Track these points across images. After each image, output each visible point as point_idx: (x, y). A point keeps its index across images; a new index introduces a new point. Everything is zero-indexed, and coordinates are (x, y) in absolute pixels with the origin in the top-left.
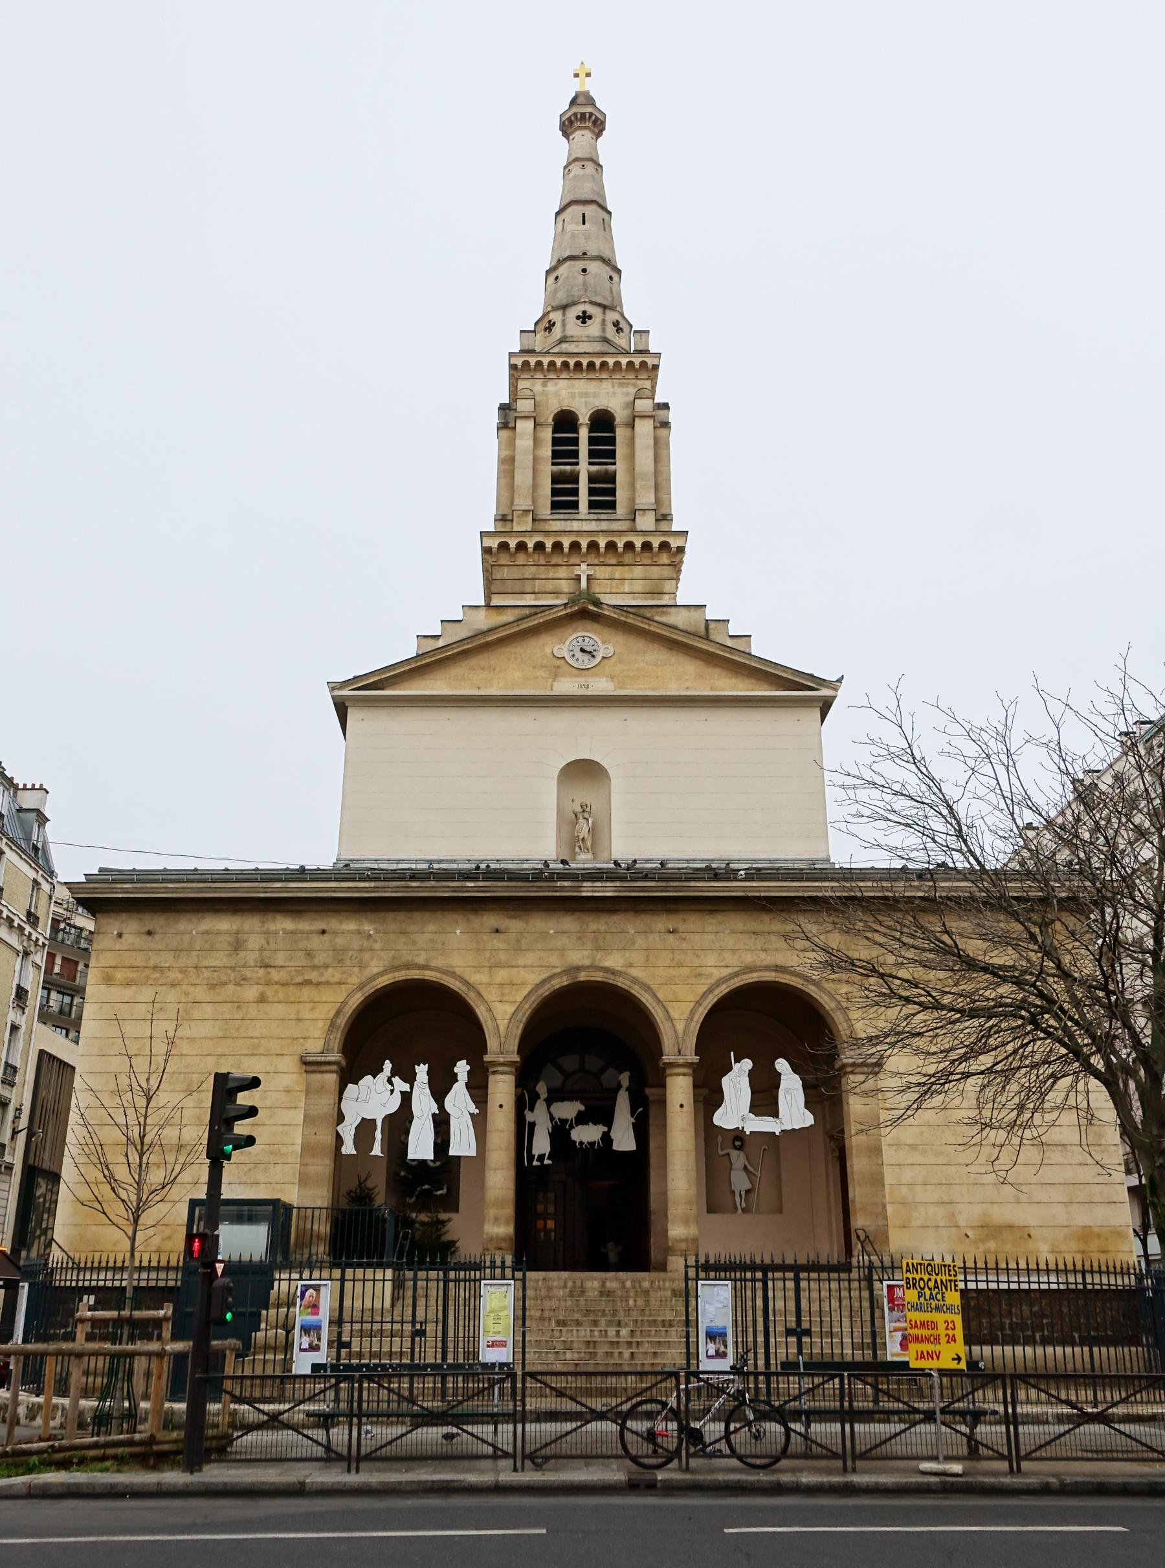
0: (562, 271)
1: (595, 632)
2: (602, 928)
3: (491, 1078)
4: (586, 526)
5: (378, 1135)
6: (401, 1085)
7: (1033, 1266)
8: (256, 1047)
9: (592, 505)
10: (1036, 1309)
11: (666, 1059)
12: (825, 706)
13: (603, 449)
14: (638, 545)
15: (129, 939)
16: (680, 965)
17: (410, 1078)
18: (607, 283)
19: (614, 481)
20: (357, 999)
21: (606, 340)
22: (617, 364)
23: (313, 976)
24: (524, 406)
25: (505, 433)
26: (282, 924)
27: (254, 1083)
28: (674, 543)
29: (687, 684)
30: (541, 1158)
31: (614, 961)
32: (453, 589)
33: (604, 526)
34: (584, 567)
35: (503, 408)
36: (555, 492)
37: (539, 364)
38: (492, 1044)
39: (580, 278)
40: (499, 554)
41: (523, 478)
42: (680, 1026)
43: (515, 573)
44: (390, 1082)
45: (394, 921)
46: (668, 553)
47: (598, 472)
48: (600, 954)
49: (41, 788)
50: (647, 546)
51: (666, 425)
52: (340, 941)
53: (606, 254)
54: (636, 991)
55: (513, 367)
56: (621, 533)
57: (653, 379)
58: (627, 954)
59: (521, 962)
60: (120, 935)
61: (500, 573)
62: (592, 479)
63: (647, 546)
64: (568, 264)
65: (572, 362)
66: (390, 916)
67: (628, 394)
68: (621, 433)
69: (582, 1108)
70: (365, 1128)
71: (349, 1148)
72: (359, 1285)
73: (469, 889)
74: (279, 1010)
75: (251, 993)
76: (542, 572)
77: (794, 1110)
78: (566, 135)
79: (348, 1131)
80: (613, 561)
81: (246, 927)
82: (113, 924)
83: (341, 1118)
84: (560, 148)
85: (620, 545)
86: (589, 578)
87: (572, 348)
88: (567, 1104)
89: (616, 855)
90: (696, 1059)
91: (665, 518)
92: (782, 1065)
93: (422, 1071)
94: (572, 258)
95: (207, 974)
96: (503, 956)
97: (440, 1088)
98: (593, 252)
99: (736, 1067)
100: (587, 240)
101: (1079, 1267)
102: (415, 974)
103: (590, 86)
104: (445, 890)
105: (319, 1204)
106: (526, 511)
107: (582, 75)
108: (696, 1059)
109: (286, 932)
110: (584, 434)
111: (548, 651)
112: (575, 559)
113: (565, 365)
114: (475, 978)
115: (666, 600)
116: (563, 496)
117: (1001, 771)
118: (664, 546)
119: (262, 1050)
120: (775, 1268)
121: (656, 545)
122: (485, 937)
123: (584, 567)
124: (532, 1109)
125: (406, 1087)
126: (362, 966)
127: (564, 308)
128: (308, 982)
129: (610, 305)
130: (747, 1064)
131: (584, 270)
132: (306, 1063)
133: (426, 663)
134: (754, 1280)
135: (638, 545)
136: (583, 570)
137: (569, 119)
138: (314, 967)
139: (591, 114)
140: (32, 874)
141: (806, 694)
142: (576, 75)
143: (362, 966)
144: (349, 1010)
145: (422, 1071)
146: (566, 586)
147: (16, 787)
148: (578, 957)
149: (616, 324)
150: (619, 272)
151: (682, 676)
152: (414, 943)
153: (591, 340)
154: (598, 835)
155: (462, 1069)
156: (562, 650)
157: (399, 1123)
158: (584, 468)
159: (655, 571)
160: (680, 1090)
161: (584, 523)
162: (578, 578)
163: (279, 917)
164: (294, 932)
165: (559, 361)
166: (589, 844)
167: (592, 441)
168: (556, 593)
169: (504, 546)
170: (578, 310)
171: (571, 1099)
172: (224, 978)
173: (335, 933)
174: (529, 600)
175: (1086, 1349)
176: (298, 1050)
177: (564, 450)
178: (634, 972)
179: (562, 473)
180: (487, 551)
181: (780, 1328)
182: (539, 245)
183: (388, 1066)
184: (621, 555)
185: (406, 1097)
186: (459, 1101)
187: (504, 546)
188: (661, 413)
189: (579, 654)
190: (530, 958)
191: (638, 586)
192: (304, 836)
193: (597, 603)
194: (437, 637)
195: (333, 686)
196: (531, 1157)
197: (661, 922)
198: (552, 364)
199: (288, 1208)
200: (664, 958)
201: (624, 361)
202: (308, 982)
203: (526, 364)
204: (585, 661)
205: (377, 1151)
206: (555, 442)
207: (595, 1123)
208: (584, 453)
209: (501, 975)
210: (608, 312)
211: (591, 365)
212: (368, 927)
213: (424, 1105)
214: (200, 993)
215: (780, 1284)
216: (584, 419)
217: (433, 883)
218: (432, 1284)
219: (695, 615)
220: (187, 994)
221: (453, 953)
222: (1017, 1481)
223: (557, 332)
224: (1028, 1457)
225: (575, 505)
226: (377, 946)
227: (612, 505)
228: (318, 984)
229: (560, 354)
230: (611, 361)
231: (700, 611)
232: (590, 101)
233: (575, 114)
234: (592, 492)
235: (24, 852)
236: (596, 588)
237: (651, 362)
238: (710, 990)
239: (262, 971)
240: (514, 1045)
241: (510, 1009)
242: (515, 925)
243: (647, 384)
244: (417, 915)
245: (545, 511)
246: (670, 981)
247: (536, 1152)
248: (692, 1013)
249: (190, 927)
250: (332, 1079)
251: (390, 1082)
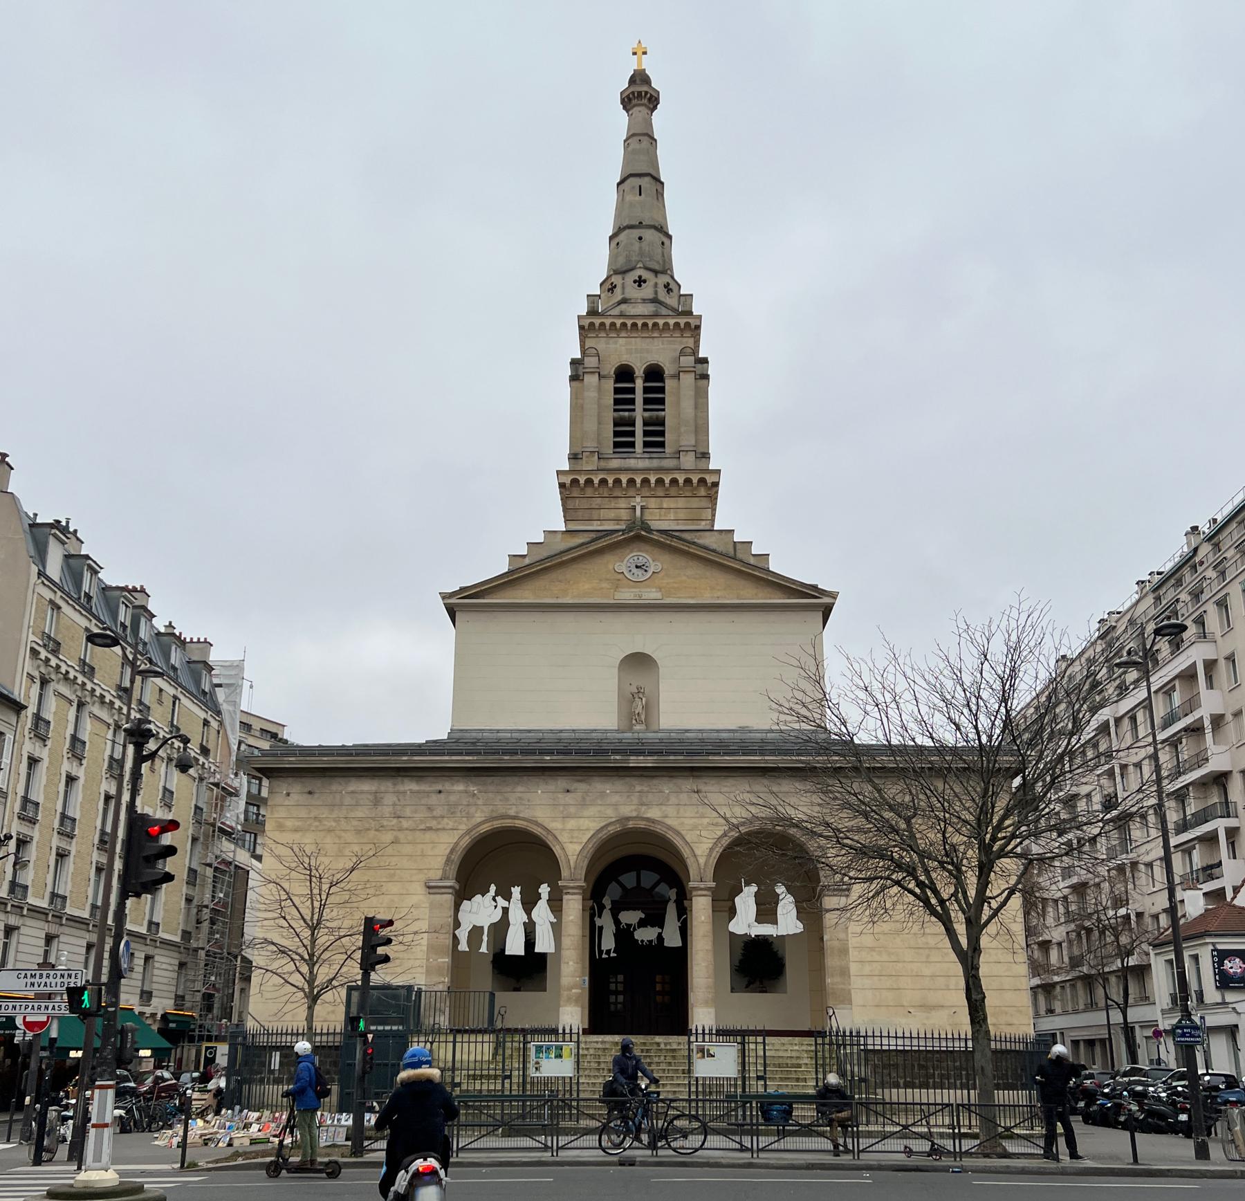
0: (622, 237)
1: (646, 552)
2: (646, 789)
4: (641, 464)
5: (485, 938)
6: (501, 902)
7: (956, 1036)
8: (394, 875)
9: (646, 444)
10: (958, 1064)
11: (691, 884)
12: (827, 611)
13: (655, 398)
14: (681, 481)
15: (295, 797)
16: (702, 817)
17: (508, 897)
19: (663, 424)
20: (466, 841)
21: (655, 301)
22: (666, 324)
23: (433, 824)
24: (591, 362)
25: (575, 384)
26: (410, 786)
27: (391, 923)
28: (710, 479)
29: (719, 594)
30: (608, 952)
31: (654, 813)
33: (655, 463)
34: (638, 499)
35: (574, 363)
36: (616, 434)
37: (602, 324)
38: (565, 873)
39: (637, 244)
40: (570, 488)
42: (702, 861)
43: (584, 504)
44: (494, 899)
45: (492, 783)
46: (707, 487)
47: (651, 417)
48: (644, 808)
49: (205, 641)
50: (688, 481)
51: (706, 377)
55: (581, 328)
56: (667, 470)
58: (664, 808)
60: (288, 794)
61: (570, 505)
63: (688, 481)
64: (627, 231)
65: (629, 322)
66: (490, 780)
67: (675, 350)
68: (669, 384)
69: (643, 916)
70: (476, 932)
71: (463, 946)
72: (465, 1045)
73: (547, 762)
74: (408, 849)
75: (388, 837)
76: (606, 503)
77: (788, 922)
79: (463, 934)
80: (662, 494)
81: (383, 789)
82: (283, 786)
83: (457, 924)
84: (621, 121)
85: (667, 481)
86: (642, 508)
88: (631, 913)
90: (713, 884)
91: (705, 456)
92: (780, 889)
93: (516, 891)
95: (355, 823)
97: (529, 903)
99: (746, 889)
102: (508, 823)
105: (440, 987)
107: (640, 53)
108: (713, 884)
109: (412, 792)
110: (639, 384)
112: (631, 492)
116: (623, 442)
118: (702, 481)
119: (396, 878)
121: (695, 481)
122: (560, 796)
123: (638, 499)
124: (600, 916)
125: (505, 904)
126: (469, 816)
128: (430, 829)
129: (664, 268)
130: (754, 888)
131: (640, 238)
132: (429, 887)
135: (681, 481)
136: (638, 501)
137: (628, 96)
138: (434, 817)
139: (646, 93)
140: (203, 715)
141: (814, 603)
142: (635, 54)
143: (469, 816)
145: (516, 891)
146: (624, 515)
147: (184, 642)
148: (628, 810)
149: (667, 286)
150: (670, 237)
151: (714, 588)
152: (507, 800)
154: (650, 708)
155: (544, 890)
157: (500, 928)
159: (695, 503)
160: (701, 907)
161: (639, 460)
162: (634, 508)
163: (406, 780)
164: (418, 792)
165: (618, 322)
166: (643, 717)
167: (646, 390)
168: (618, 520)
171: (634, 909)
172: (367, 826)
173: (449, 792)
174: (596, 526)
175: (965, 1092)
176: (422, 877)
177: (623, 399)
178: (669, 822)
179: (622, 418)
180: (562, 486)
181: (753, 1075)
183: (493, 888)
184: (667, 490)
185: (505, 911)
186: (542, 913)
187: (575, 482)
189: (635, 570)
190: (592, 811)
192: (426, 721)
193: (649, 530)
194: (523, 556)
195: (445, 596)
196: (601, 952)
200: (690, 812)
202: (430, 829)
203: (592, 324)
204: (640, 575)
205: (484, 949)
207: (652, 926)
208: (639, 393)
209: (572, 824)
210: (651, 296)
212: (473, 788)
213: (517, 916)
214: (349, 837)
215: (752, 1046)
216: (639, 372)
217: (520, 757)
218: (486, 1045)
220: (340, 837)
223: (618, 295)
225: (632, 445)
226: (480, 802)
228: (438, 830)
229: (622, 315)
230: (661, 322)
231: (729, 535)
233: (633, 93)
234: (646, 434)
235: (195, 697)
236: (647, 516)
237: (693, 323)
239: (395, 821)
241: (578, 848)
245: (609, 449)
247: (604, 948)
248: (711, 849)
249: (340, 788)
250: (448, 899)
251: (494, 899)
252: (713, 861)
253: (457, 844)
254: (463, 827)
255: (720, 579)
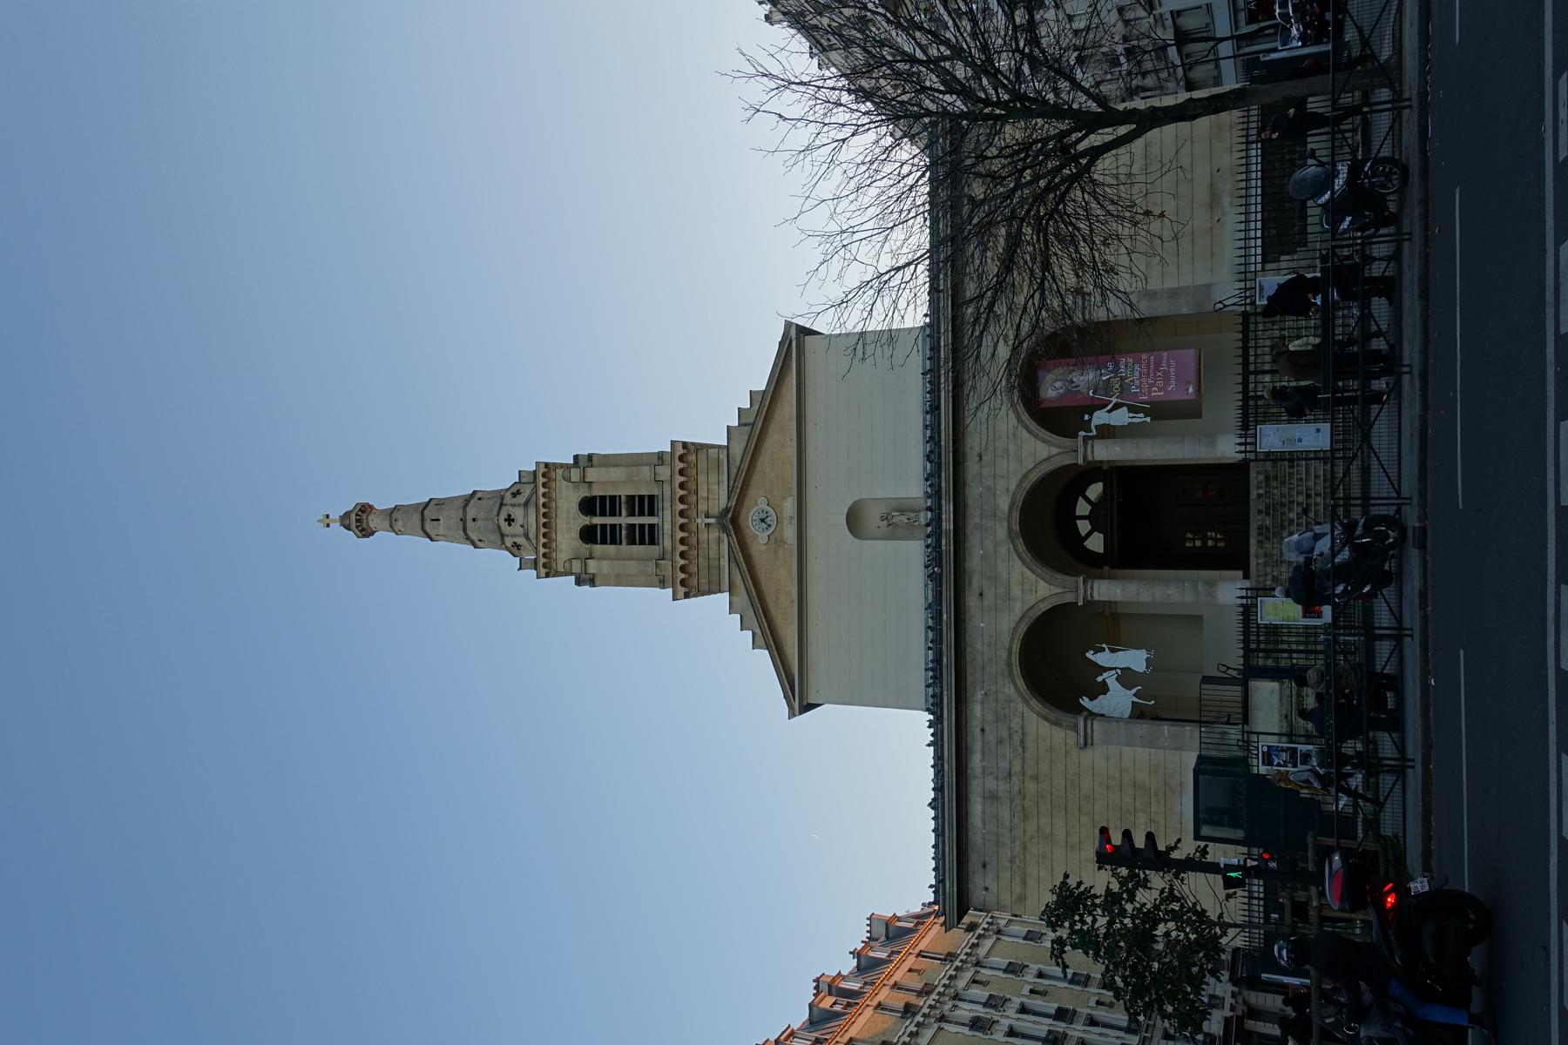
0: (473, 536)
3: (1096, 597)
4: (668, 518)
9: (651, 513)
10: (1277, 165)
12: (804, 332)
13: (608, 505)
15: (989, 882)
16: (1007, 451)
18: (484, 502)
21: (526, 504)
22: (544, 495)
23: (1017, 738)
25: (597, 581)
26: (976, 762)
27: (1104, 831)
28: (680, 451)
31: (1004, 503)
32: (715, 613)
33: (667, 504)
35: (579, 582)
36: (642, 542)
37: (544, 555)
39: (479, 523)
40: (689, 586)
41: (616, 474)
42: (1054, 451)
46: (687, 454)
50: (682, 472)
51: (590, 457)
52: (989, 717)
53: (460, 503)
54: (1027, 485)
57: (556, 466)
59: (1005, 576)
61: (705, 587)
62: (631, 514)
68: (597, 492)
75: (1031, 786)
78: (372, 533)
81: (979, 790)
84: (383, 537)
85: (682, 493)
86: (707, 516)
87: (533, 530)
89: (921, 495)
91: (660, 455)
94: (465, 529)
95: (1016, 821)
96: (1001, 590)
98: (460, 514)
100: (451, 517)
101: (1243, 147)
102: (1015, 659)
103: (336, 514)
104: (949, 636)
106: (657, 566)
109: (983, 760)
110: (597, 520)
111: (763, 548)
113: (545, 535)
114: (1018, 613)
115: (723, 457)
116: (648, 536)
117: (857, 236)
120: (1245, 391)
121: (681, 465)
126: (1009, 700)
127: (502, 536)
128: (1022, 742)
129: (500, 498)
133: (769, 638)
134: (1256, 406)
144: (1045, 711)
146: (714, 534)
148: (1001, 531)
149: (514, 495)
151: (781, 442)
153: (526, 515)
156: (763, 537)
158: (624, 520)
159: (702, 465)
161: (665, 520)
162: (707, 525)
163: (970, 765)
164: (983, 754)
165: (543, 540)
167: (603, 514)
168: (719, 541)
169: (683, 583)
170: (504, 525)
173: (984, 720)
174: (725, 562)
177: (610, 536)
178: (1013, 487)
179: (628, 537)
182: (454, 552)
187: (683, 583)
188: (582, 462)
190: (1002, 569)
191: (713, 477)
193: (727, 510)
195: (792, 715)
197: (972, 468)
198: (544, 545)
199: (1201, 759)
201: (542, 490)
202: (1022, 742)
203: (544, 565)
206: (604, 542)
209: (1016, 591)
211: (545, 515)
212: (979, 695)
214: (1031, 827)
216: (586, 520)
219: (734, 434)
221: (997, 626)
222: (1417, 632)
223: (521, 541)
224: (1398, 492)
225: (652, 527)
226: (993, 688)
227: (652, 498)
230: (542, 500)
232: (347, 514)
234: (641, 514)
236: (715, 511)
237: (542, 469)
238: (1026, 427)
239: (1014, 779)
240: (1070, 580)
241: (1042, 584)
242: (976, 582)
243: (559, 472)
244: (968, 657)
245: (654, 550)
246: (1019, 460)
252: (1056, 438)
253: (1039, 714)
254: (1021, 707)
255: (773, 438)
